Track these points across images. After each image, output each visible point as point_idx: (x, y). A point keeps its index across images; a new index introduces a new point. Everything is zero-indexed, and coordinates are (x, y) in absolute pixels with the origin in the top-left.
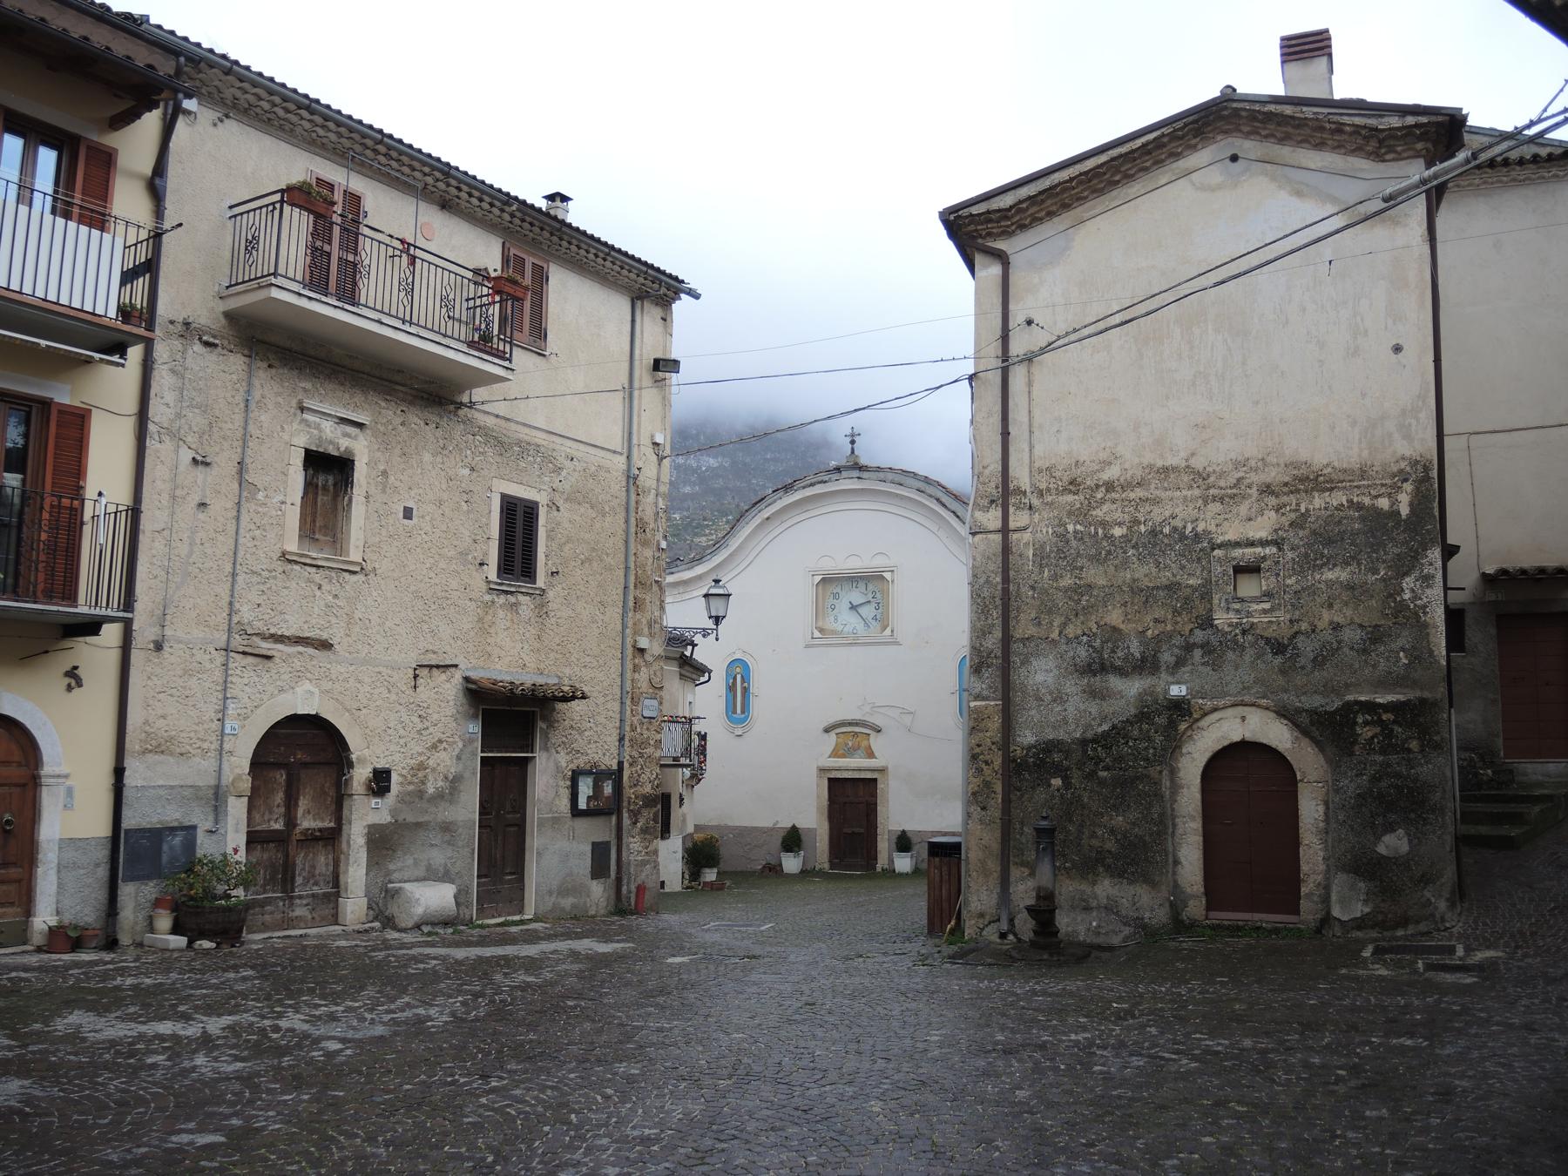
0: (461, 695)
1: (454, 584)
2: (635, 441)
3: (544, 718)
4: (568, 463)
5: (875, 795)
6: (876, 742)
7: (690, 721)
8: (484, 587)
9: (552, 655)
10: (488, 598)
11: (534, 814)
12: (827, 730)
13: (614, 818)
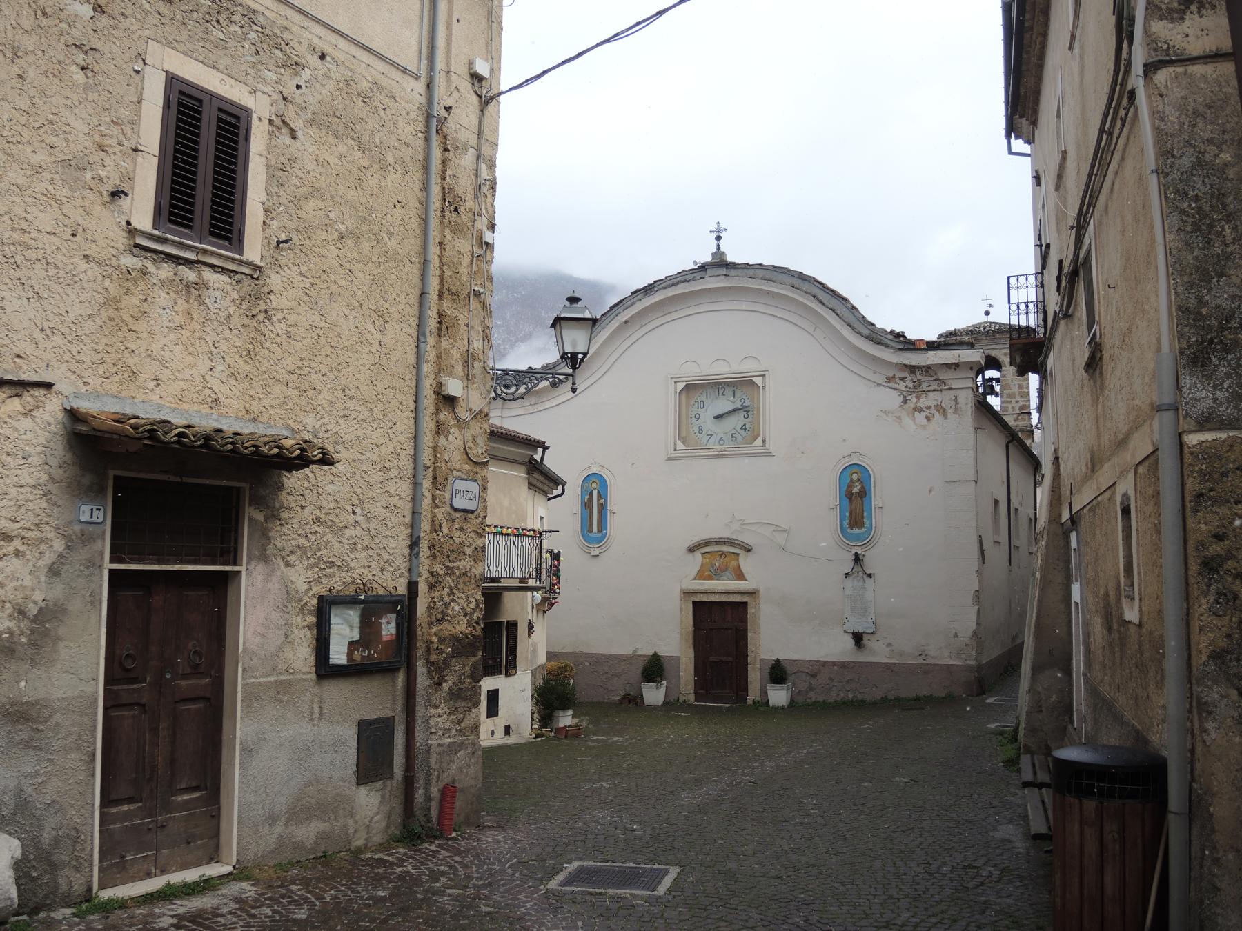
0: (59, 447)
1: (45, 220)
2: (440, 64)
3: (258, 502)
4: (314, 60)
5: (744, 621)
6: (746, 563)
7: (538, 535)
8: (122, 240)
9: (277, 390)
10: (129, 261)
11: (243, 677)
13: (401, 677)
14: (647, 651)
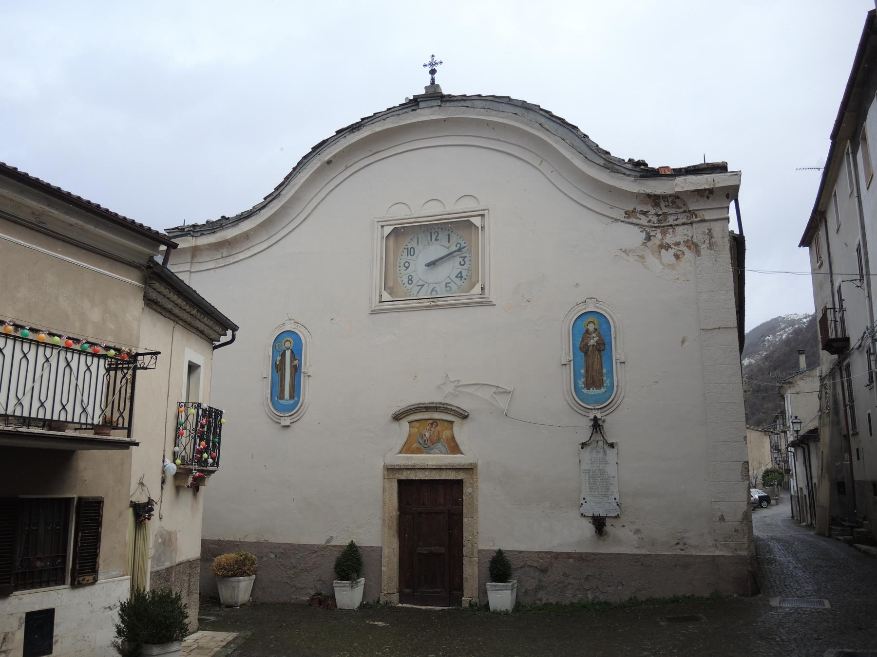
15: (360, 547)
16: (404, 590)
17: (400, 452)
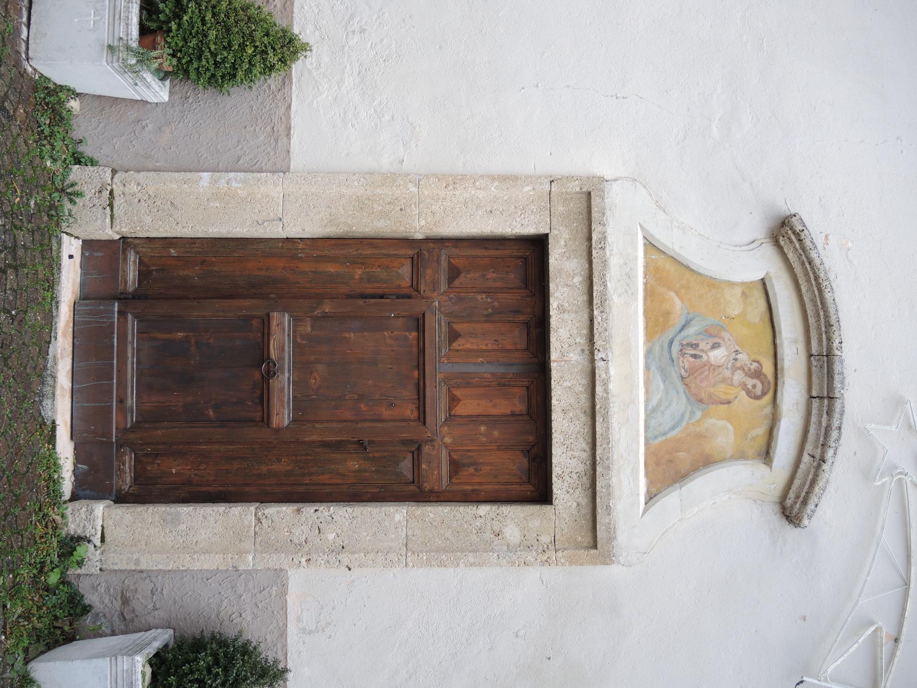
12: (785, 233)
14: (290, 666)
15: (287, 81)
16: (132, 257)
17: (651, 245)
